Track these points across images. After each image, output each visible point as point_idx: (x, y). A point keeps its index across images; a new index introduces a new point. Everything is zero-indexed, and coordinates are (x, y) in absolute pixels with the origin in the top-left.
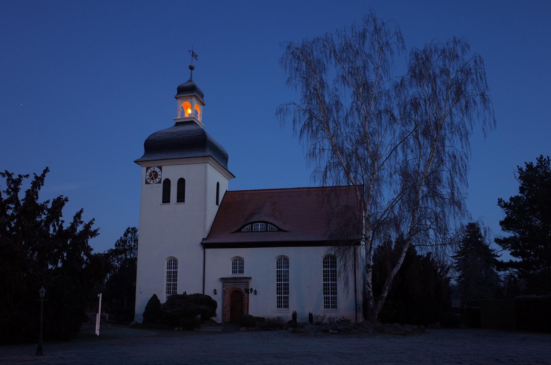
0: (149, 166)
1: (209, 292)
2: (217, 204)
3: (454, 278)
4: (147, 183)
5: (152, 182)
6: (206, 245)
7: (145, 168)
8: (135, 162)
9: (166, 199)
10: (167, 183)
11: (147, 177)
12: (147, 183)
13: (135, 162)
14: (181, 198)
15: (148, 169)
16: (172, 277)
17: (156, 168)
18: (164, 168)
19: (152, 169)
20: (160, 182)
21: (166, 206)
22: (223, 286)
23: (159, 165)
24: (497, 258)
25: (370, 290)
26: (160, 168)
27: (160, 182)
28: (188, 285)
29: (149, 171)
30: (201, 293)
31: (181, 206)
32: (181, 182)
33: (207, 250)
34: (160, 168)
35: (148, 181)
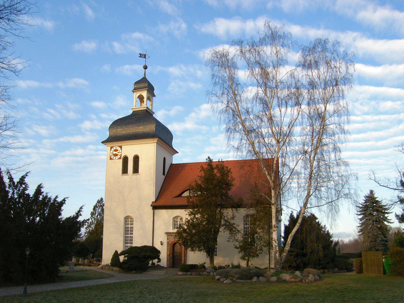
0: (112, 146)
1: (158, 246)
2: (164, 174)
3: (184, 215)
4: (111, 159)
5: (114, 158)
6: (155, 207)
7: (110, 147)
8: (102, 143)
9: (125, 171)
10: (125, 160)
11: (111, 154)
12: (111, 159)
13: (102, 143)
14: (136, 170)
15: (111, 148)
16: (128, 232)
17: (118, 147)
18: (123, 147)
19: (114, 148)
20: (120, 158)
21: (125, 177)
22: (168, 239)
23: (120, 145)
24: (386, 223)
25: (277, 245)
26: (121, 147)
27: (120, 158)
28: (140, 240)
29: (112, 149)
30: (151, 245)
31: (136, 176)
32: (136, 159)
33: (157, 211)
34: (121, 147)
35: (112, 157)
